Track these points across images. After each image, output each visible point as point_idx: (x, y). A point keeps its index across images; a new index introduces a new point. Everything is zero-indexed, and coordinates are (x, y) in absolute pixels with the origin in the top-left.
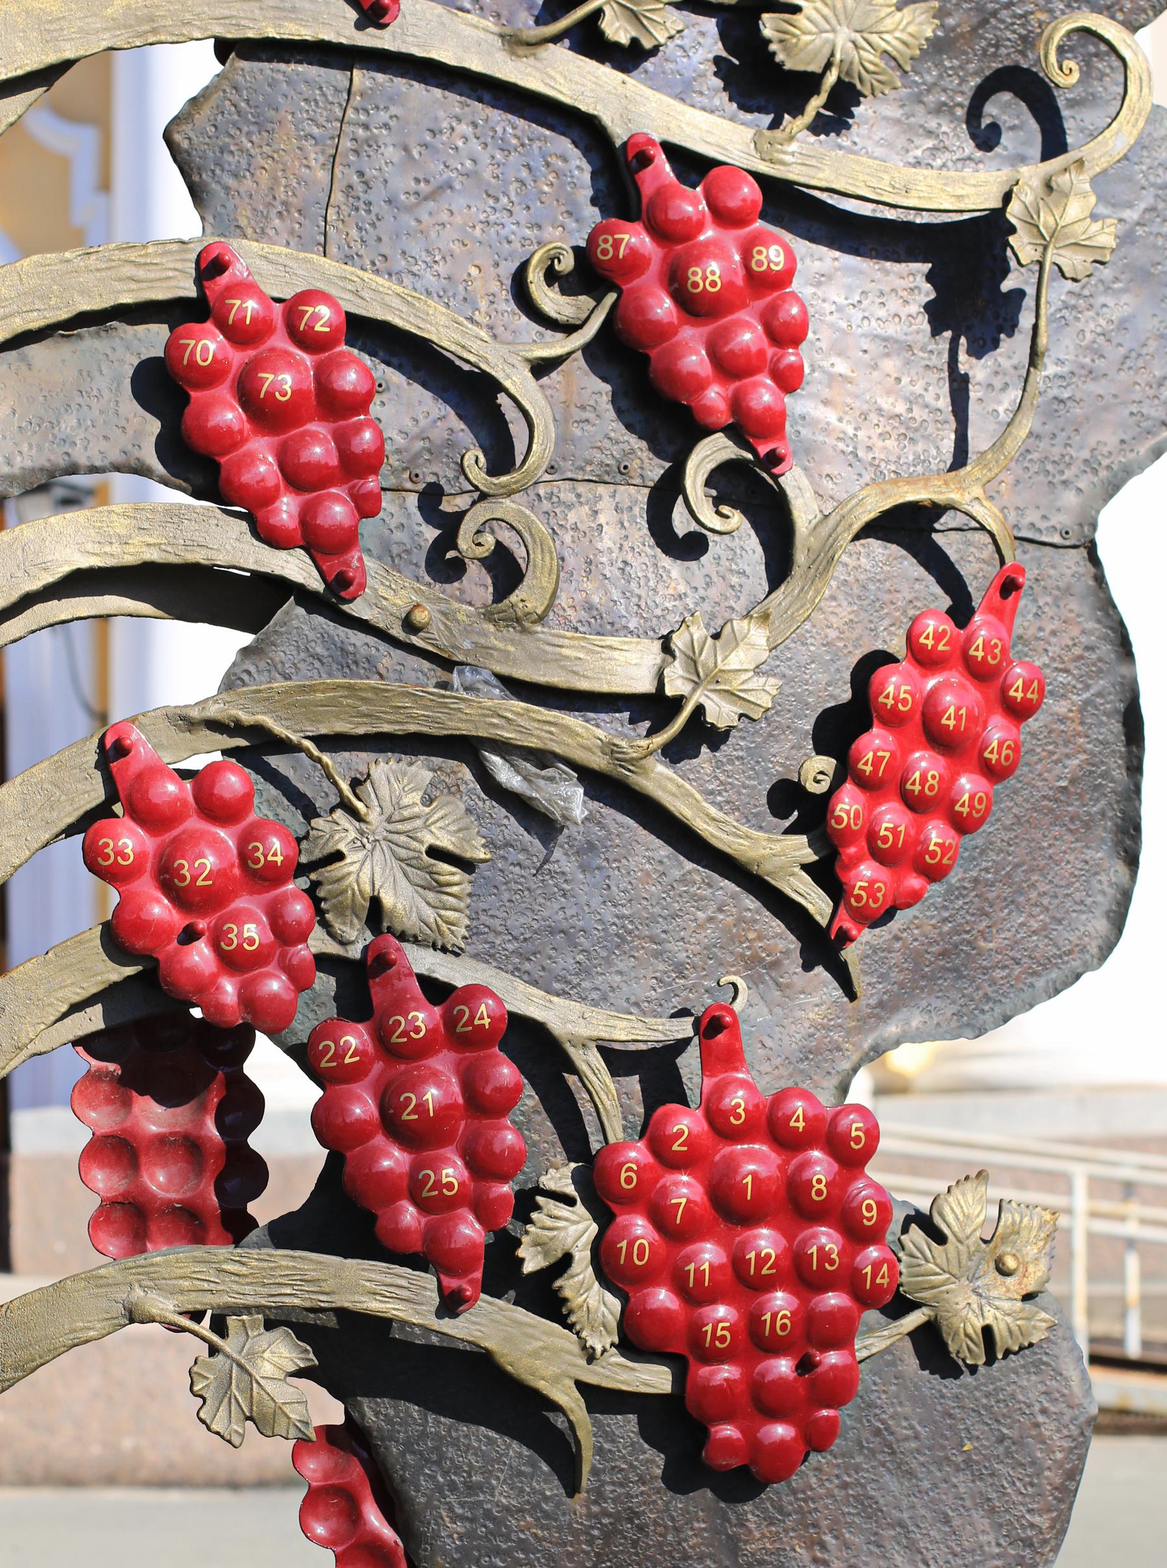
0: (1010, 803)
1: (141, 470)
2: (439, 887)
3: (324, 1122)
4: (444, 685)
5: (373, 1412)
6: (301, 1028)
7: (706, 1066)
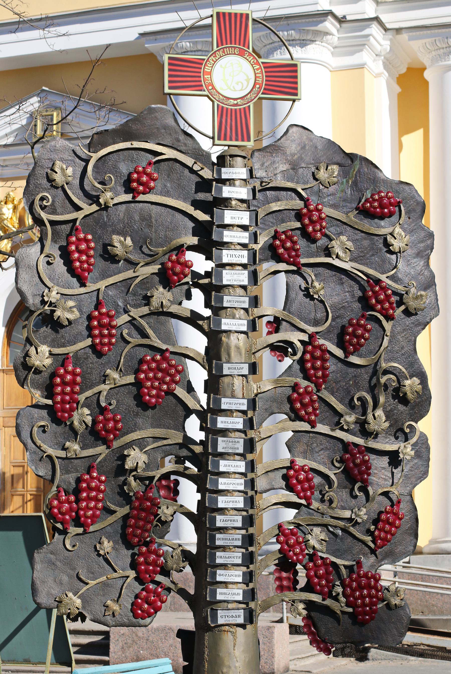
0: (399, 532)
1: (283, 489)
2: (322, 544)
3: (307, 576)
4: (323, 517)
5: (313, 614)
6: (304, 563)
7: (357, 568)
